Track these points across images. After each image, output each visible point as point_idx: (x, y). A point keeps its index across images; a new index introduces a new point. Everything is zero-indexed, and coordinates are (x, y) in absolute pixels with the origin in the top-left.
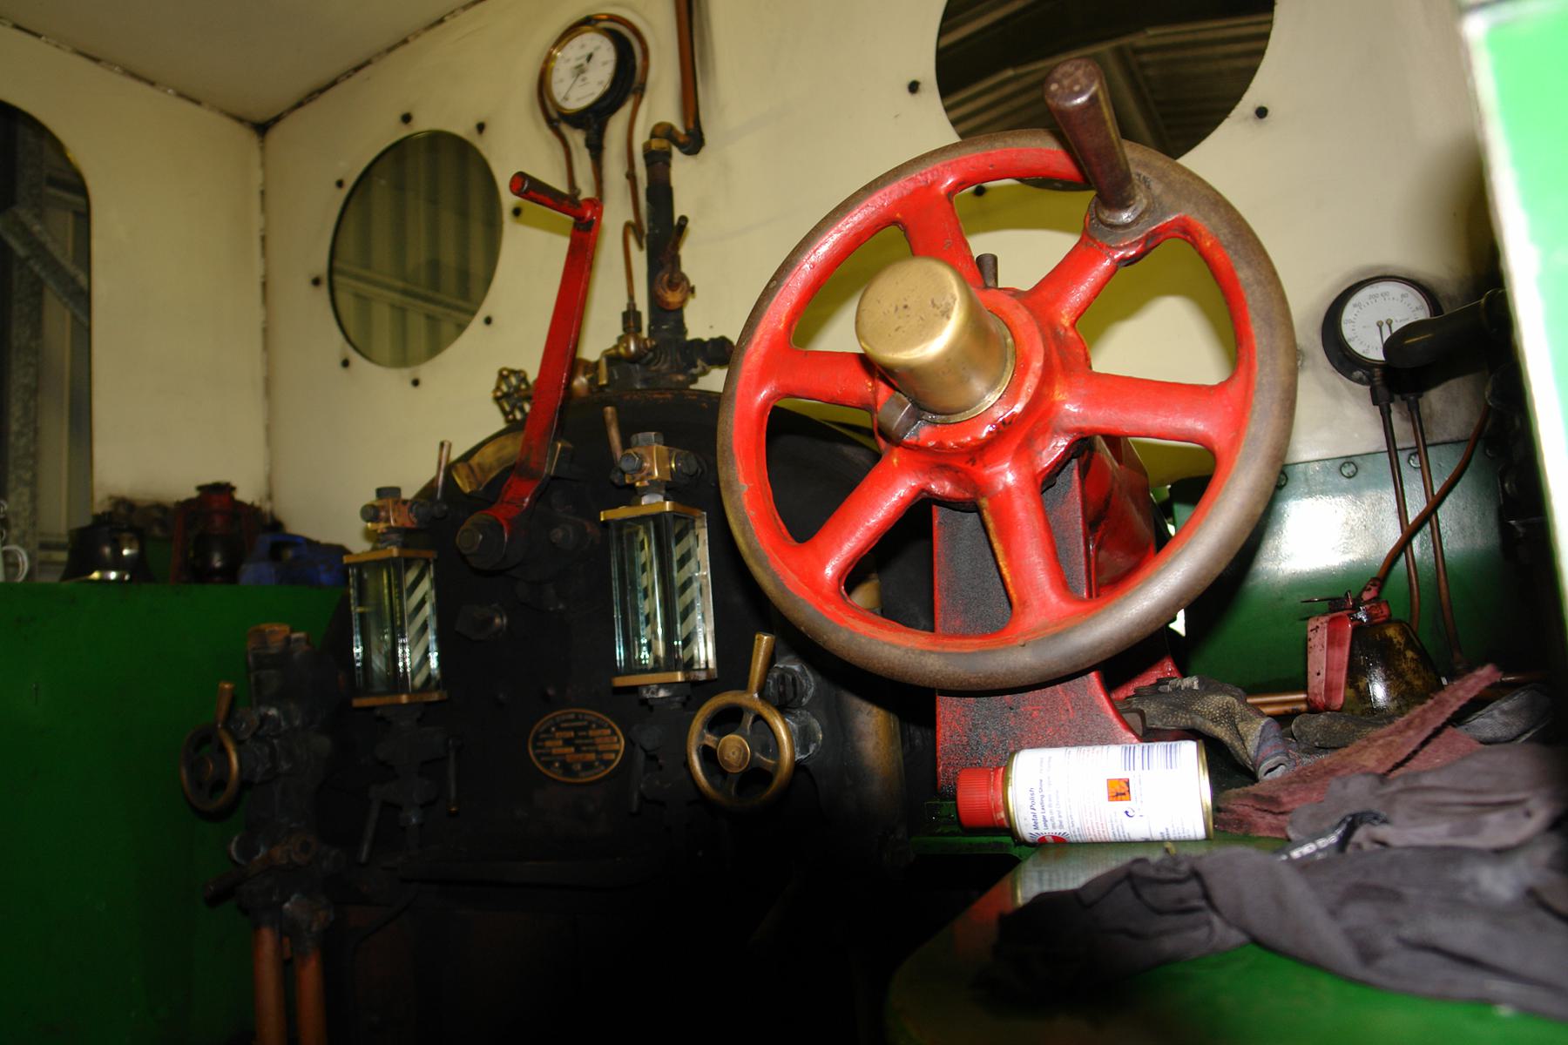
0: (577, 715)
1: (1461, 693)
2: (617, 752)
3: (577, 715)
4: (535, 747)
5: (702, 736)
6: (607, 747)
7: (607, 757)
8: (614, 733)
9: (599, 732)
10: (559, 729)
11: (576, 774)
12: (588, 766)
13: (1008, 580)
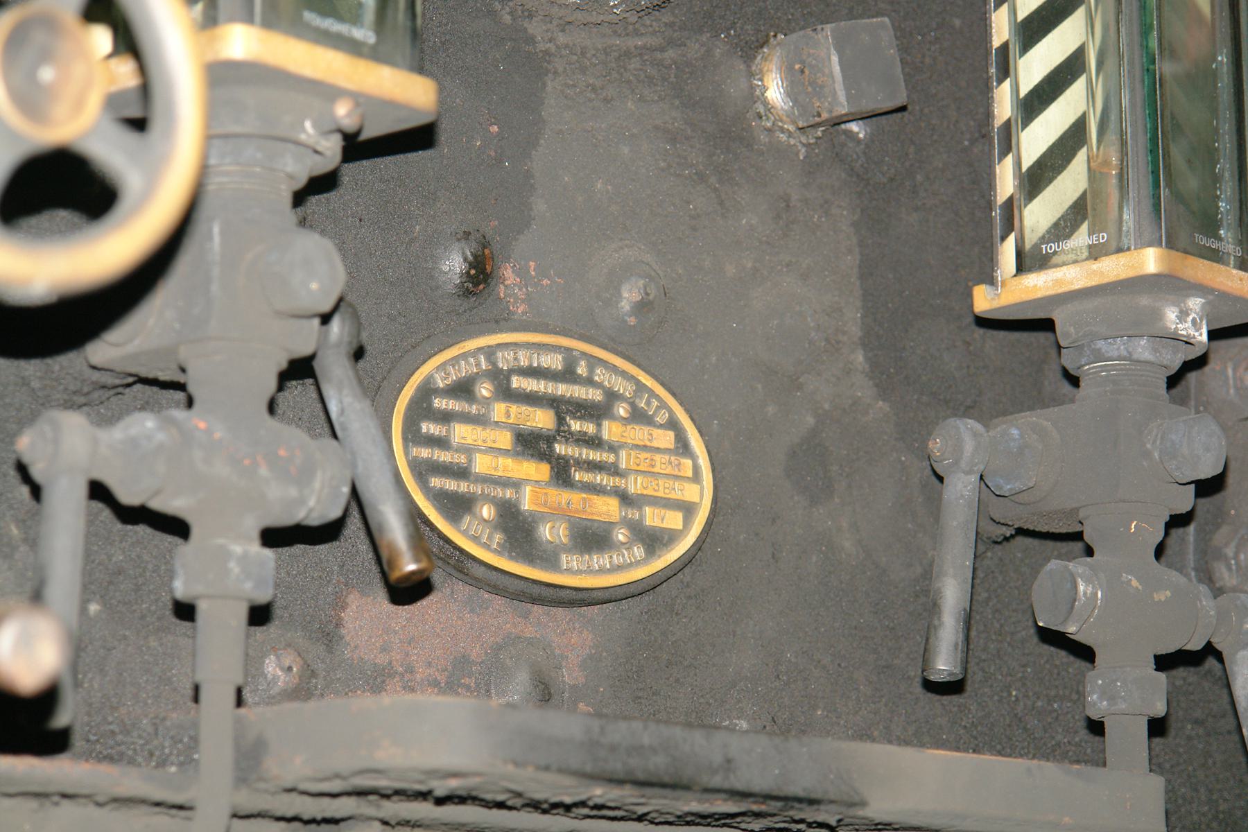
0: (571, 359)
1: (570, 450)
2: (688, 509)
3: (571, 359)
4: (412, 435)
5: (406, 454)
6: (662, 489)
7: (652, 517)
8: (683, 447)
9: (638, 434)
10: (507, 394)
11: (549, 559)
12: (591, 538)
13: (695, 807)
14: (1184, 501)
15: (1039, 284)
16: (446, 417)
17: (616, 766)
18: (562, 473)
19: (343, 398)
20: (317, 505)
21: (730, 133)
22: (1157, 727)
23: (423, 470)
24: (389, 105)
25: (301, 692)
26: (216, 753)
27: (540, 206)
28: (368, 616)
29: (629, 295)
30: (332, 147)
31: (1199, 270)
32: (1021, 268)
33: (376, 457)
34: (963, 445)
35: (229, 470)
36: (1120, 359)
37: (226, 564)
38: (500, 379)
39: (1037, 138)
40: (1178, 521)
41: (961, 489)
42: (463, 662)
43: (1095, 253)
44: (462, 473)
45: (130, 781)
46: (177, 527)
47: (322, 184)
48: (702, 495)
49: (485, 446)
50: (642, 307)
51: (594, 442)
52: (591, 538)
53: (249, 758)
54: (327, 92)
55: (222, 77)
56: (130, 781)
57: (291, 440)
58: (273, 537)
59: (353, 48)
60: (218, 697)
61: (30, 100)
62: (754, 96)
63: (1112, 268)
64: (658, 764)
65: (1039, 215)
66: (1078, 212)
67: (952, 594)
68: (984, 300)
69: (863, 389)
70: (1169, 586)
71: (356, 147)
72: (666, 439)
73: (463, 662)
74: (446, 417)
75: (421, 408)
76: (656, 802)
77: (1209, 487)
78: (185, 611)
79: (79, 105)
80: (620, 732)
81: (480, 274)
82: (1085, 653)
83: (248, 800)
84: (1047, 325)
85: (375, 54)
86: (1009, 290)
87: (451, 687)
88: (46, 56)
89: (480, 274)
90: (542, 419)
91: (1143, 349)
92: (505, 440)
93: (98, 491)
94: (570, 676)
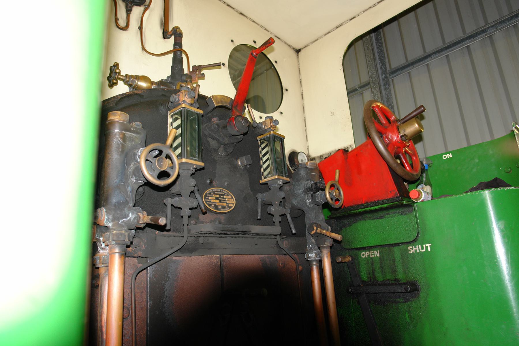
2: (233, 204)
4: (205, 198)
6: (230, 202)
7: (229, 205)
8: (232, 198)
9: (228, 197)
11: (219, 210)
12: (224, 207)
14: (281, 200)
15: (266, 180)
16: (208, 196)
17: (226, 229)
18: (220, 201)
19: (197, 195)
20: (195, 205)
21: (235, 167)
22: (280, 222)
23: (206, 202)
24: (199, 166)
25: (196, 224)
26: (186, 231)
27: (217, 175)
28: (201, 217)
29: (226, 183)
30: (194, 170)
31: (281, 177)
32: (264, 178)
33: (202, 201)
34: (260, 196)
35: (186, 203)
36: (273, 186)
37: (186, 212)
38: (214, 192)
39: (265, 166)
40: (281, 202)
41: (260, 200)
42: (211, 220)
43: (271, 176)
44: (210, 202)
45: (177, 234)
46: (181, 208)
47: (193, 174)
48: (234, 202)
49: (212, 199)
50: (228, 184)
51: (223, 198)
52: (224, 207)
53: (189, 231)
54: (193, 165)
55: (180, 164)
56: (177, 234)
57: (192, 199)
58: (190, 209)
59: (196, 160)
60: (186, 225)
61: (160, 166)
62: (238, 164)
63: (273, 178)
64: (230, 229)
65: (266, 173)
66: (269, 173)
67: (259, 210)
68: (261, 182)
69: (250, 191)
70: (280, 208)
71: (197, 170)
72: (231, 197)
73: (211, 220)
74: (208, 196)
75: (206, 196)
76: (230, 233)
77: (283, 198)
78: (182, 217)
79: (166, 166)
80: (226, 226)
81: (211, 182)
82: (273, 215)
83: (189, 235)
84: (267, 184)
85: (198, 161)
86: (263, 180)
87: (210, 223)
88: (162, 162)
89: (211, 182)
90: (218, 196)
91: (276, 185)
92: (214, 198)
93: (172, 205)
94: (222, 221)
